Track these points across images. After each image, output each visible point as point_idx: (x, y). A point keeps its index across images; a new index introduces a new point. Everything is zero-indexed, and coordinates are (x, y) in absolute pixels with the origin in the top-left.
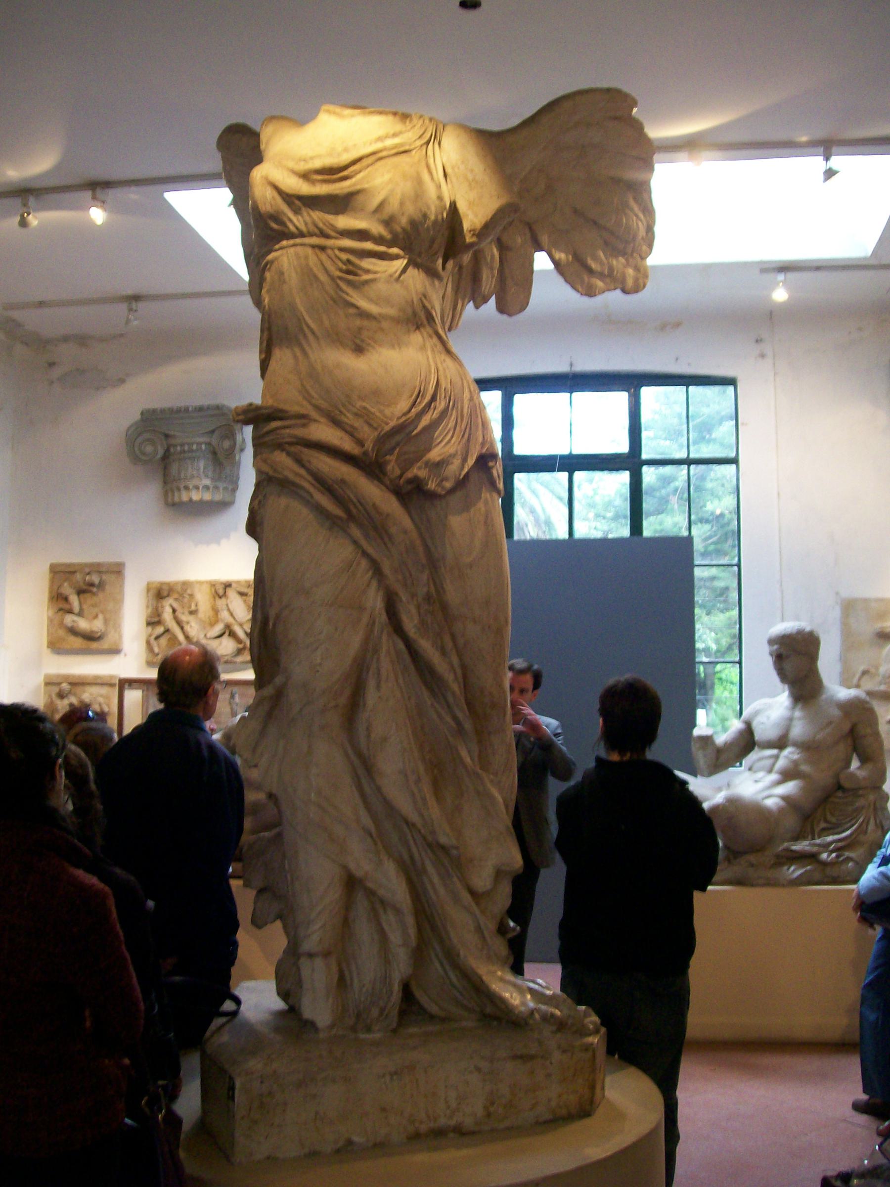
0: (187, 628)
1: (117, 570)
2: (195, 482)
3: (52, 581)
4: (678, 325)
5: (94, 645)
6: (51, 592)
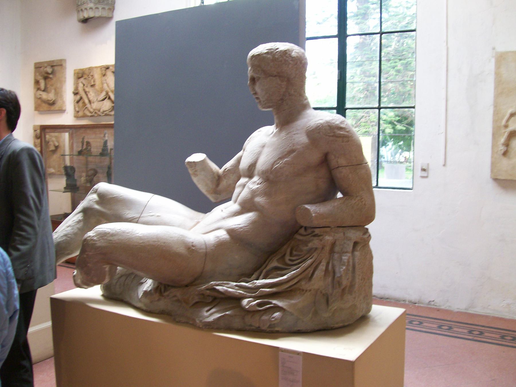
5: (53, 108)
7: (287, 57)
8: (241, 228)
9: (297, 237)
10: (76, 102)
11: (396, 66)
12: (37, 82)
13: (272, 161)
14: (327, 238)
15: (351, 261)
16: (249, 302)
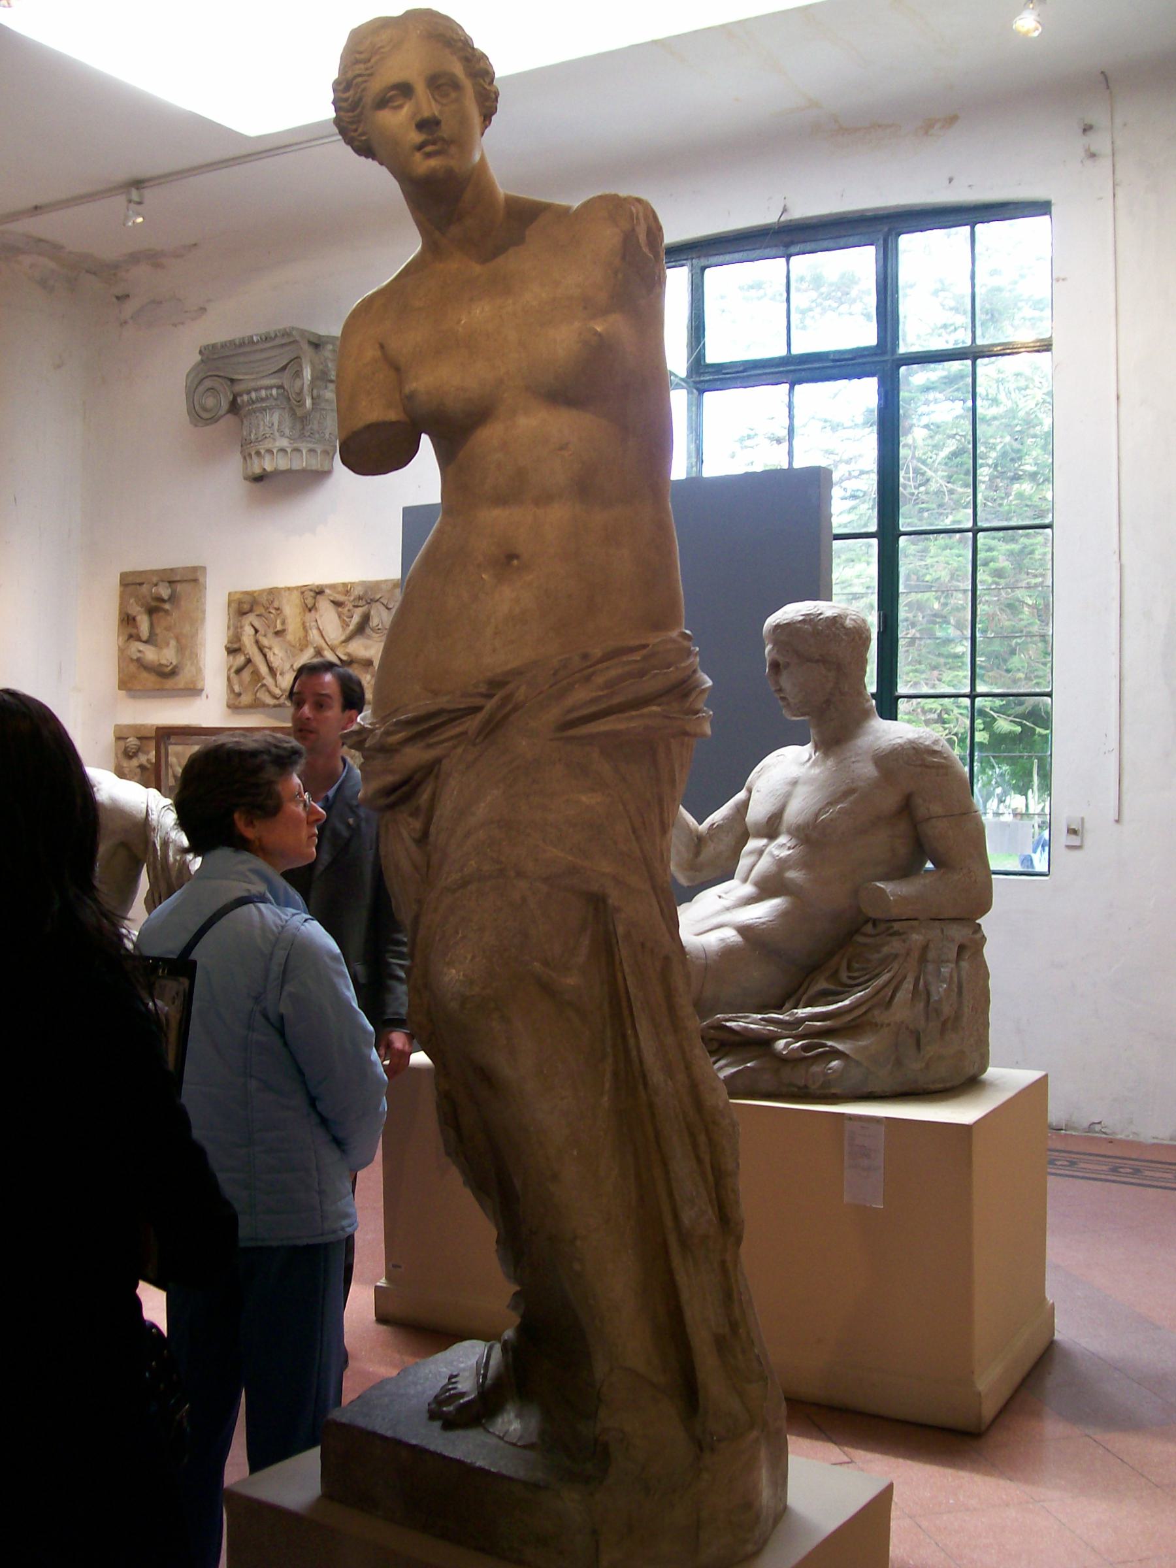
2: (268, 444)
4: (952, 120)
5: (169, 683)
7: (837, 629)
8: (763, 923)
9: (860, 939)
10: (233, 670)
11: (993, 560)
12: (127, 620)
13: (818, 807)
14: (915, 937)
15: (955, 975)
16: (787, 1045)
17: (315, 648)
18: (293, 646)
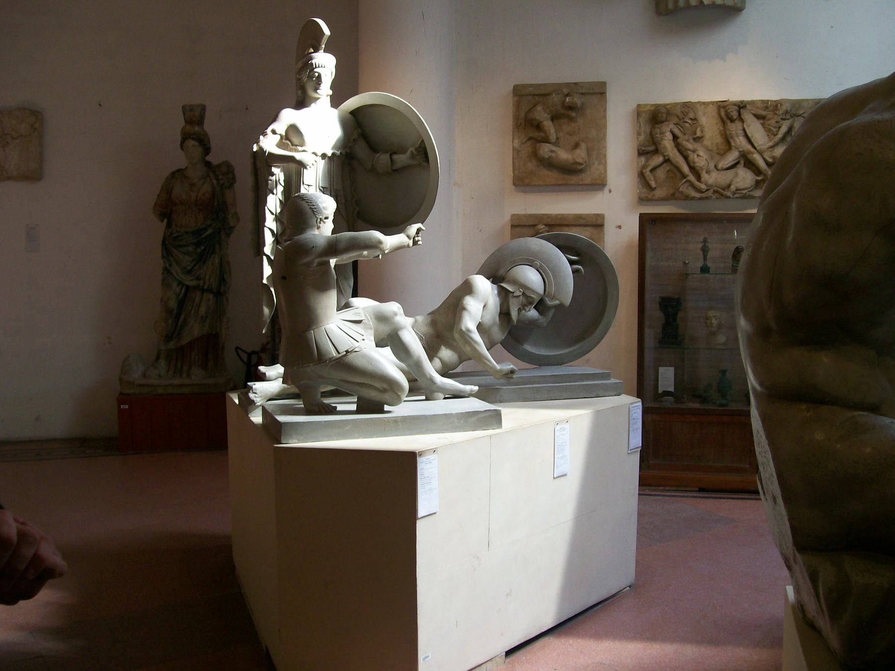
0: (693, 157)
1: (598, 91)
3: (517, 106)
5: (574, 179)
6: (516, 118)
17: (740, 152)
18: (710, 150)
